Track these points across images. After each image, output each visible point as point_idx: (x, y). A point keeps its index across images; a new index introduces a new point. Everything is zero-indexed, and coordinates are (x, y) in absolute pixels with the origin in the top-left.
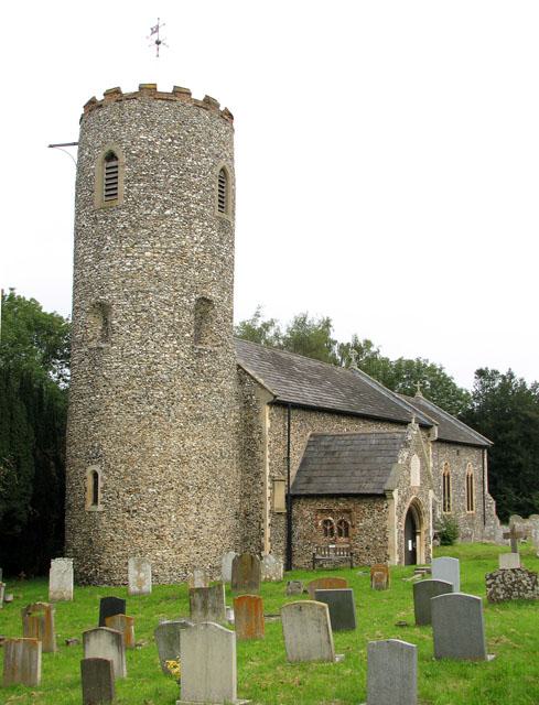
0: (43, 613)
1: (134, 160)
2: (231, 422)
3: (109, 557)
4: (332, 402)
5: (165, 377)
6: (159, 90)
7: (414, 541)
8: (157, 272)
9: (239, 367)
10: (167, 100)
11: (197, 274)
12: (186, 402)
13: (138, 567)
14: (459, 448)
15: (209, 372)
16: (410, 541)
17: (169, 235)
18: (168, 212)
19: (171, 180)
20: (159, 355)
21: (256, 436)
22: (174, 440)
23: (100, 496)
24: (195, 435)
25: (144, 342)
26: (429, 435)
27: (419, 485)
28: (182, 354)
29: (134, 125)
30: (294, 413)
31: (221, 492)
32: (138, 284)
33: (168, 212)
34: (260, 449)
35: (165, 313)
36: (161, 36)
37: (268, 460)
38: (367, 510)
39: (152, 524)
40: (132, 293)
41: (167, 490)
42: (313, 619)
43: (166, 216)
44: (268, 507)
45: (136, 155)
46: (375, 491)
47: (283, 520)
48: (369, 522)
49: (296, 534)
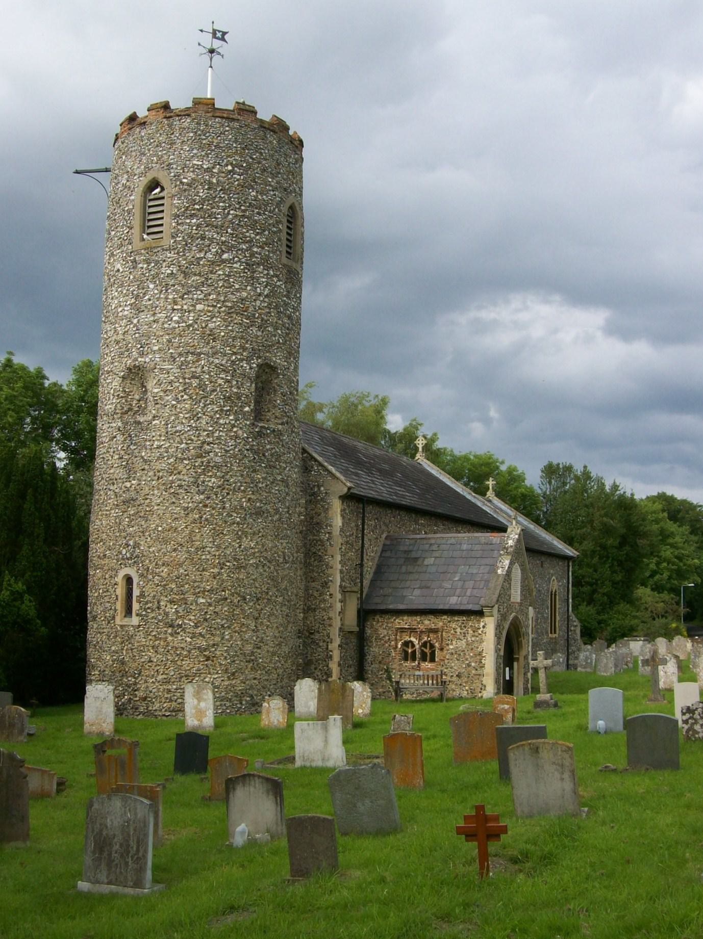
0: (124, 751)
2: (295, 519)
3: (146, 682)
4: (409, 499)
6: (216, 106)
7: (511, 669)
9: (304, 451)
10: (227, 118)
11: (259, 333)
12: (244, 491)
13: (198, 695)
14: (543, 559)
15: (272, 455)
16: (507, 669)
18: (225, 256)
19: (230, 217)
23: (136, 606)
24: (254, 534)
27: (519, 601)
28: (240, 432)
29: (186, 148)
30: (369, 508)
31: (283, 605)
32: (188, 344)
33: (225, 256)
34: (329, 552)
36: (208, 41)
37: (339, 567)
38: (459, 630)
40: (180, 355)
42: (554, 763)
43: (224, 261)
46: (470, 607)
47: (354, 640)
48: (462, 644)
49: (369, 658)
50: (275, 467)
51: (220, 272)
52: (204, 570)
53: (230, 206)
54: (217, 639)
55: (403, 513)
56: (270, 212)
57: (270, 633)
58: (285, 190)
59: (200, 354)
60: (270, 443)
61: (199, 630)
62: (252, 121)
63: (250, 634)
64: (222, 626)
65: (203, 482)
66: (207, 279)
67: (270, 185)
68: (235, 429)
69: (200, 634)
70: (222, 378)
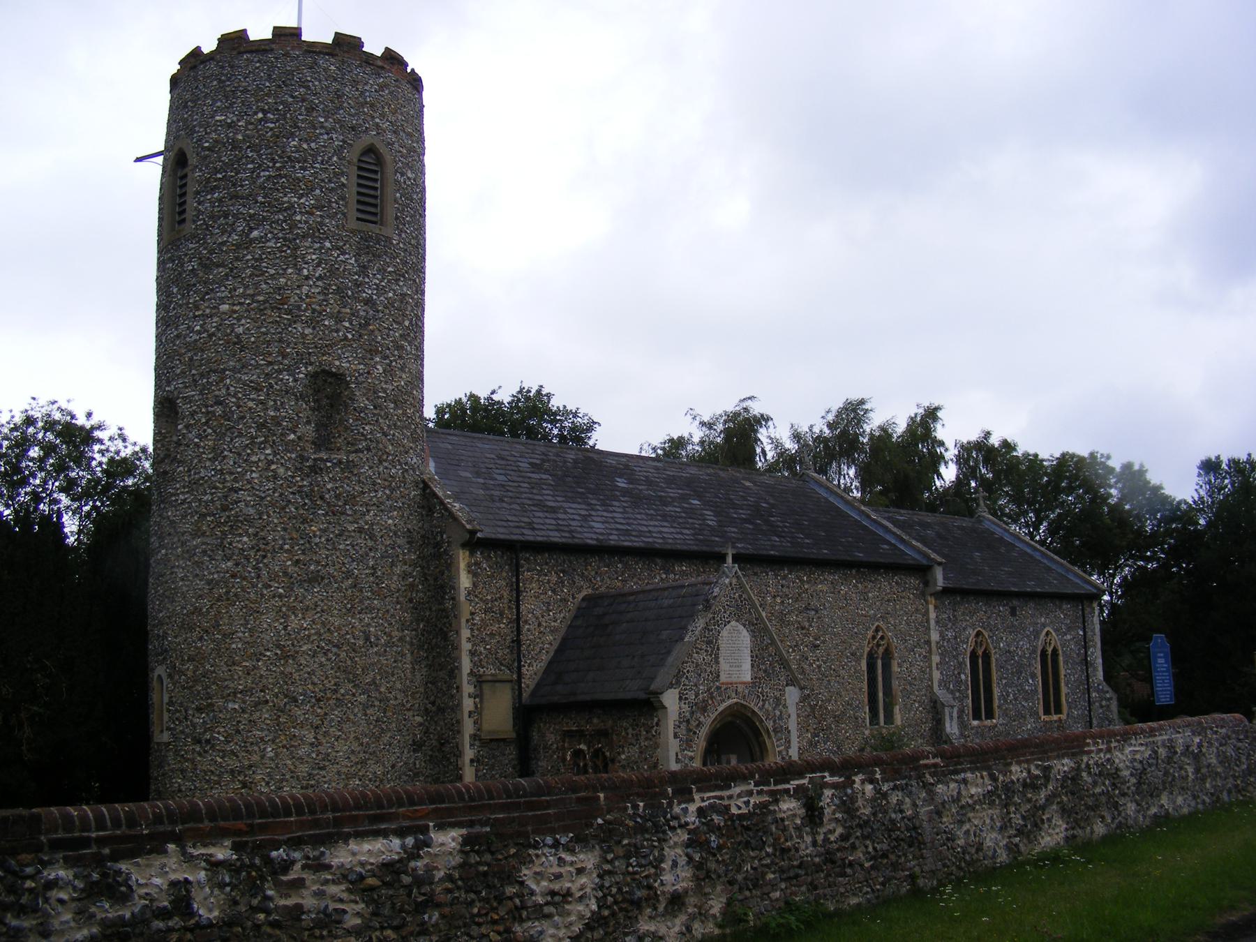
1: (206, 157)
5: (252, 511)
8: (238, 336)
14: (1015, 602)
17: (258, 271)
20: (243, 474)
21: (449, 605)
22: (267, 619)
25: (218, 455)
26: (926, 584)
27: (747, 677)
28: (281, 471)
32: (209, 360)
33: (255, 234)
35: (251, 404)
38: (630, 731)
39: (233, 763)
40: (202, 376)
41: (256, 704)
43: (252, 241)
44: (468, 727)
45: (208, 149)
50: (343, 513)
51: (249, 257)
52: (234, 664)
53: (260, 166)
54: (255, 758)
55: (594, 561)
56: (322, 163)
57: (342, 747)
58: (353, 128)
59: (224, 370)
60: (333, 480)
61: (232, 746)
62: (293, 48)
63: (307, 748)
64: (262, 739)
65: (230, 544)
66: (231, 270)
67: (322, 127)
68: (273, 467)
69: (232, 751)
70: (253, 400)
